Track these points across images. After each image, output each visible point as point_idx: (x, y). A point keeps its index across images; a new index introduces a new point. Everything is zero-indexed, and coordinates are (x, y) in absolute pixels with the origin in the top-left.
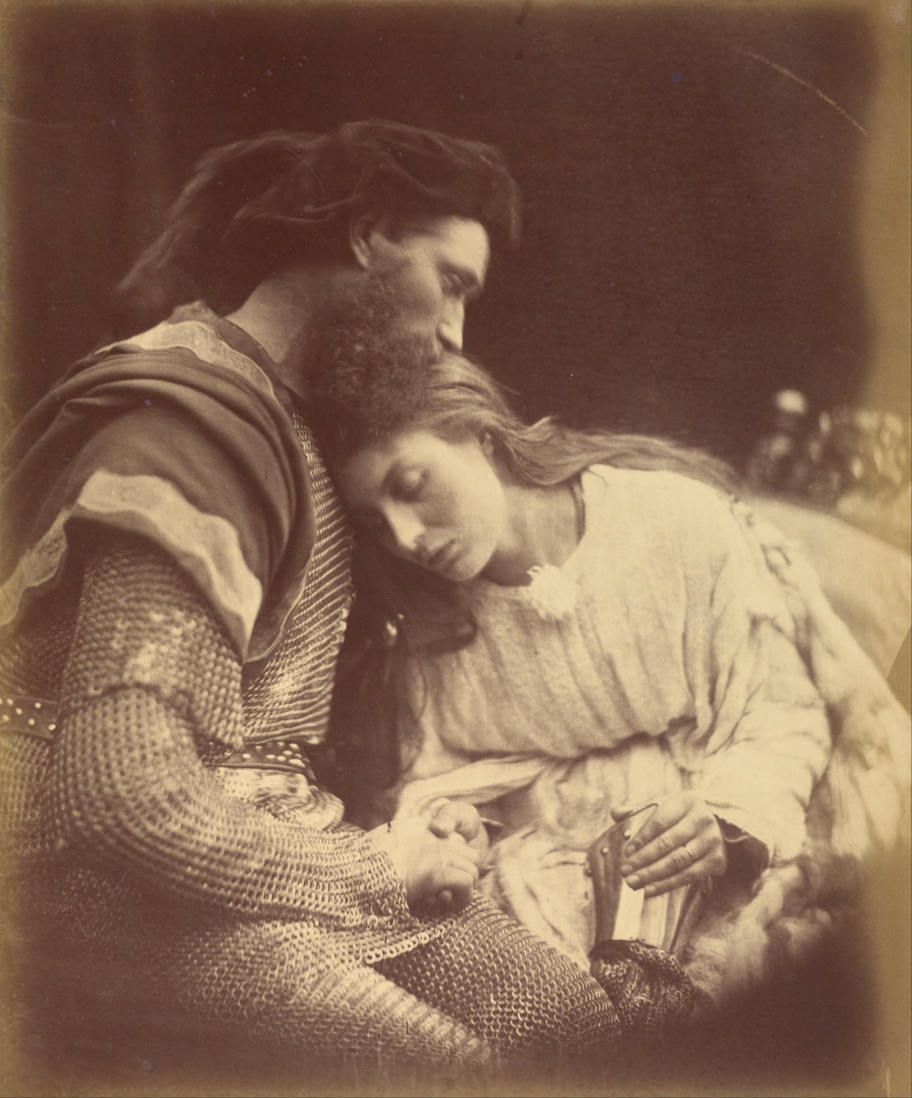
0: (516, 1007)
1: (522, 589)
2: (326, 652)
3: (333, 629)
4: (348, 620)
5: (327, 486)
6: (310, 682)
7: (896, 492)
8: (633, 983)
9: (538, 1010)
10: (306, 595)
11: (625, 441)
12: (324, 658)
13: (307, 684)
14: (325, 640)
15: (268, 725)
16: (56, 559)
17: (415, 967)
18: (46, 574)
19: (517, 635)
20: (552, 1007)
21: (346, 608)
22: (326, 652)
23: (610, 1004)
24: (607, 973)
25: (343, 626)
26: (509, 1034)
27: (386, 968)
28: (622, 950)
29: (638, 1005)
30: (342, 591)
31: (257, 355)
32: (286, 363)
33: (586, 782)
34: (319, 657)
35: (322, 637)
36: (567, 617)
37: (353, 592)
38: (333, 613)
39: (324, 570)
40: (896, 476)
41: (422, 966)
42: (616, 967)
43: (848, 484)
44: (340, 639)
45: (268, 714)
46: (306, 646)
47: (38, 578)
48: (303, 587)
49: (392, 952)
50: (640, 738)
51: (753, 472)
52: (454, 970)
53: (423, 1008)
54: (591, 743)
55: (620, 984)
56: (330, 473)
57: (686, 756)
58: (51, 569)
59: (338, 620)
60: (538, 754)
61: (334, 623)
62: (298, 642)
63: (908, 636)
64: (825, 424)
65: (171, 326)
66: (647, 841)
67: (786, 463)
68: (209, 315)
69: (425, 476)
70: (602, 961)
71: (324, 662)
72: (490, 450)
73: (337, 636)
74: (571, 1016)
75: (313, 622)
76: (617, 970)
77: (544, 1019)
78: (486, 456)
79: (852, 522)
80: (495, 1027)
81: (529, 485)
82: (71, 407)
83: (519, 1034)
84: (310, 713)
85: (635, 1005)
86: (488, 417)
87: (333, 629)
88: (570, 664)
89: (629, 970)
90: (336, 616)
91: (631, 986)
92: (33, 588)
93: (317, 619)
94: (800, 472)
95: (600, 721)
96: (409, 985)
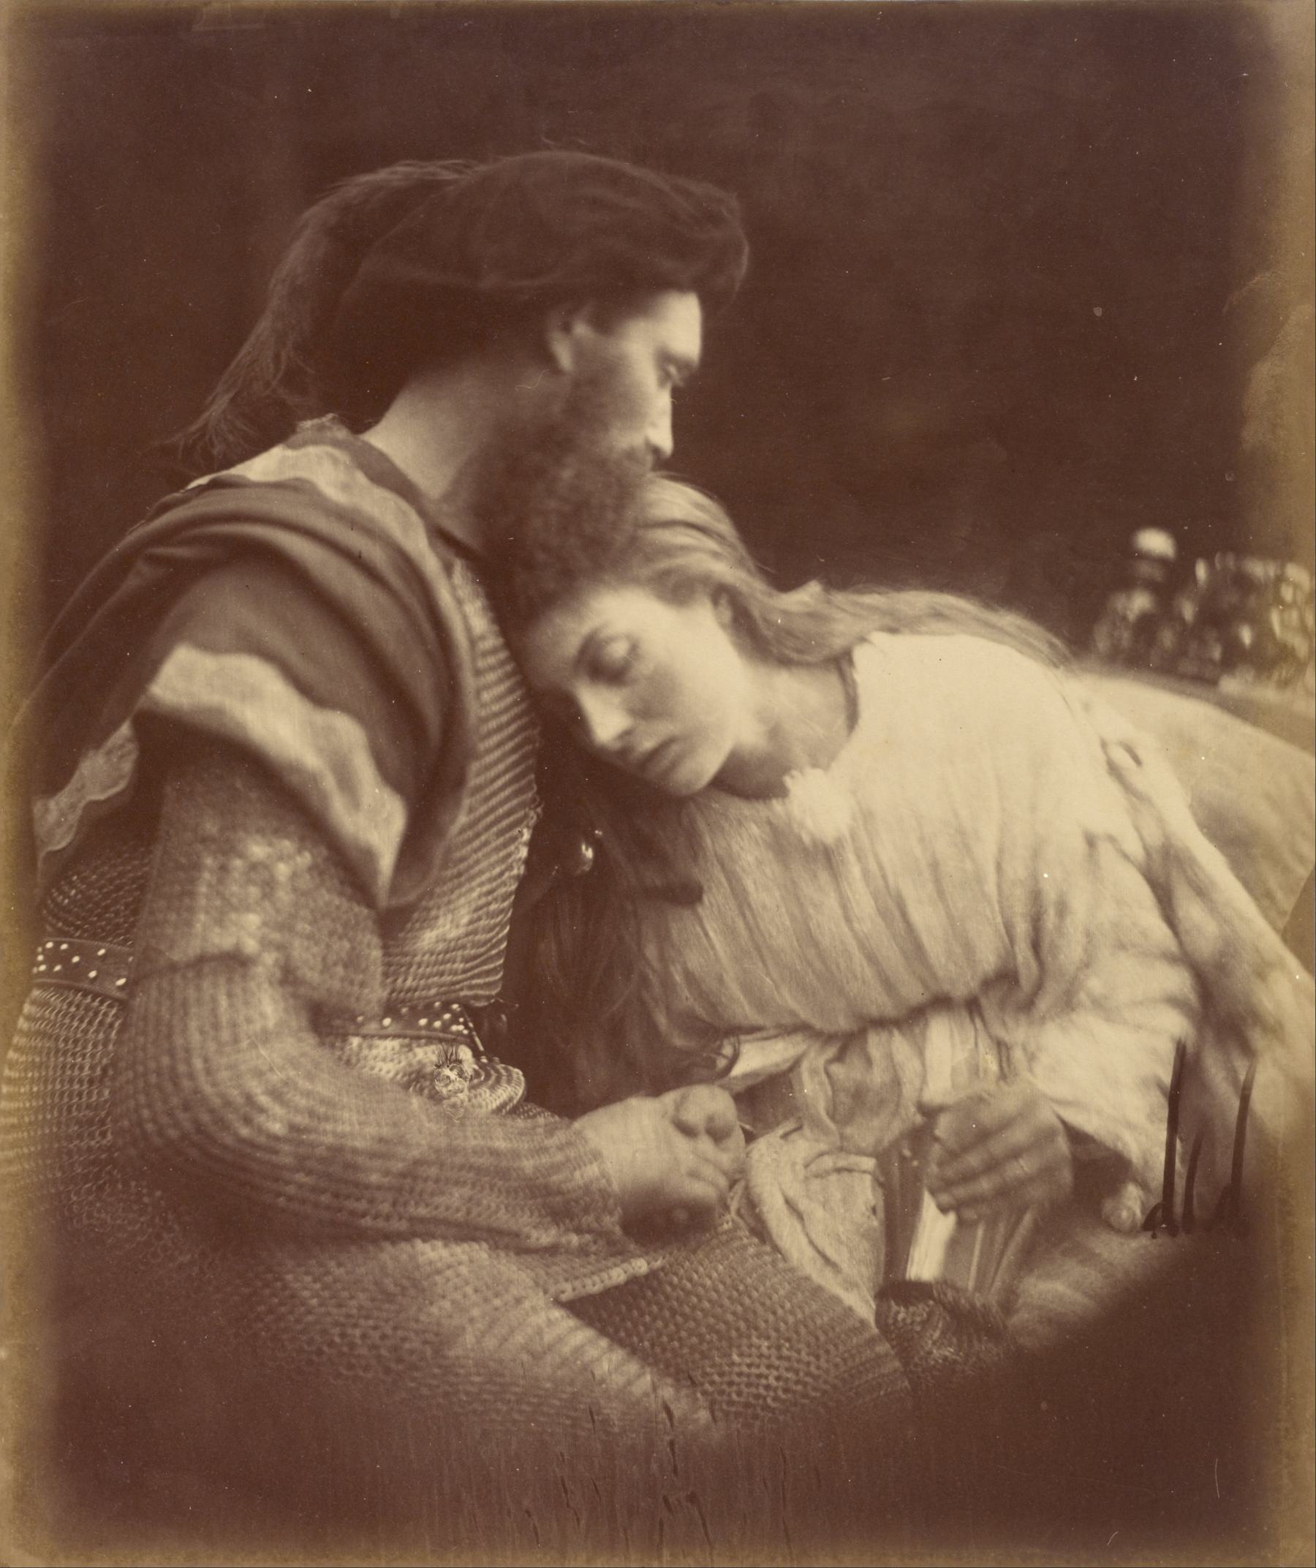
0: (769, 1367)
1: (777, 805)
2: (498, 887)
3: (509, 855)
4: (532, 844)
5: (502, 664)
6: (475, 925)
7: (1300, 667)
8: (934, 1331)
9: (797, 1372)
10: (471, 810)
11: (916, 600)
12: (495, 894)
13: (471, 927)
14: (498, 870)
15: (414, 984)
16: (127, 766)
17: (629, 1310)
18: (115, 784)
19: (772, 869)
20: (818, 1368)
21: (528, 827)
22: (498, 887)
23: (897, 1364)
24: (901, 1317)
25: (524, 852)
26: (768, 1396)
27: (581, 1308)
28: (919, 1291)
29: (940, 1361)
30: (522, 805)
31: (403, 488)
32: (447, 497)
33: (869, 1061)
34: (490, 892)
35: (493, 866)
36: (839, 842)
37: (537, 807)
38: (507, 836)
39: (498, 777)
40: (1301, 646)
41: (639, 1309)
42: (912, 1309)
43: (1234, 658)
44: (519, 870)
45: (414, 967)
46: (472, 878)
47: (105, 789)
48: (467, 802)
49: (594, 1285)
50: (941, 1002)
51: (1102, 643)
52: (683, 1315)
53: (633, 1367)
54: (874, 1011)
55: (917, 1332)
56: (508, 645)
57: (1004, 1024)
58: (121, 777)
59: (516, 844)
60: (801, 1028)
61: (512, 848)
62: (460, 875)
63: (1312, 872)
64: (1201, 571)
65: (289, 453)
66: (965, 1149)
67: (1146, 626)
68: (342, 433)
69: (634, 648)
70: (893, 1303)
71: (495, 900)
72: (727, 614)
73: (515, 865)
74: (844, 1380)
75: (479, 849)
76: (913, 1314)
77: (805, 1384)
78: (723, 626)
79: (1238, 709)
80: (739, 1394)
81: (785, 662)
82: (155, 560)
83: (783, 1396)
84: (477, 966)
85: (937, 1362)
86: (725, 570)
87: (509, 855)
88: (844, 906)
89: (930, 1314)
90: (514, 839)
91: (932, 1336)
92: (97, 803)
93: (486, 843)
94: (1167, 638)
95: (888, 984)
96: (622, 1334)
